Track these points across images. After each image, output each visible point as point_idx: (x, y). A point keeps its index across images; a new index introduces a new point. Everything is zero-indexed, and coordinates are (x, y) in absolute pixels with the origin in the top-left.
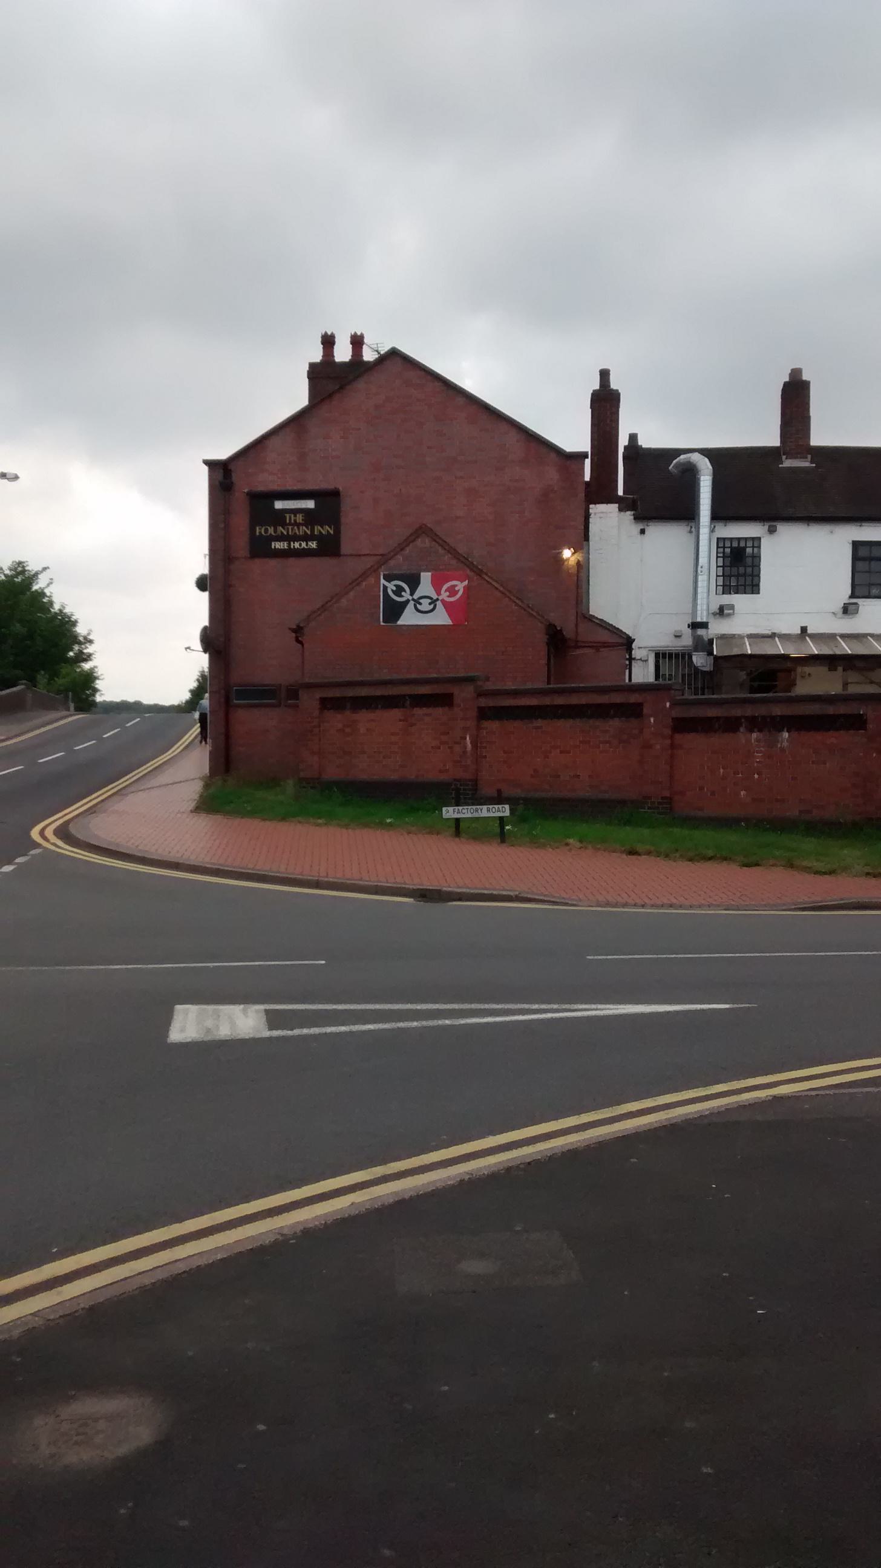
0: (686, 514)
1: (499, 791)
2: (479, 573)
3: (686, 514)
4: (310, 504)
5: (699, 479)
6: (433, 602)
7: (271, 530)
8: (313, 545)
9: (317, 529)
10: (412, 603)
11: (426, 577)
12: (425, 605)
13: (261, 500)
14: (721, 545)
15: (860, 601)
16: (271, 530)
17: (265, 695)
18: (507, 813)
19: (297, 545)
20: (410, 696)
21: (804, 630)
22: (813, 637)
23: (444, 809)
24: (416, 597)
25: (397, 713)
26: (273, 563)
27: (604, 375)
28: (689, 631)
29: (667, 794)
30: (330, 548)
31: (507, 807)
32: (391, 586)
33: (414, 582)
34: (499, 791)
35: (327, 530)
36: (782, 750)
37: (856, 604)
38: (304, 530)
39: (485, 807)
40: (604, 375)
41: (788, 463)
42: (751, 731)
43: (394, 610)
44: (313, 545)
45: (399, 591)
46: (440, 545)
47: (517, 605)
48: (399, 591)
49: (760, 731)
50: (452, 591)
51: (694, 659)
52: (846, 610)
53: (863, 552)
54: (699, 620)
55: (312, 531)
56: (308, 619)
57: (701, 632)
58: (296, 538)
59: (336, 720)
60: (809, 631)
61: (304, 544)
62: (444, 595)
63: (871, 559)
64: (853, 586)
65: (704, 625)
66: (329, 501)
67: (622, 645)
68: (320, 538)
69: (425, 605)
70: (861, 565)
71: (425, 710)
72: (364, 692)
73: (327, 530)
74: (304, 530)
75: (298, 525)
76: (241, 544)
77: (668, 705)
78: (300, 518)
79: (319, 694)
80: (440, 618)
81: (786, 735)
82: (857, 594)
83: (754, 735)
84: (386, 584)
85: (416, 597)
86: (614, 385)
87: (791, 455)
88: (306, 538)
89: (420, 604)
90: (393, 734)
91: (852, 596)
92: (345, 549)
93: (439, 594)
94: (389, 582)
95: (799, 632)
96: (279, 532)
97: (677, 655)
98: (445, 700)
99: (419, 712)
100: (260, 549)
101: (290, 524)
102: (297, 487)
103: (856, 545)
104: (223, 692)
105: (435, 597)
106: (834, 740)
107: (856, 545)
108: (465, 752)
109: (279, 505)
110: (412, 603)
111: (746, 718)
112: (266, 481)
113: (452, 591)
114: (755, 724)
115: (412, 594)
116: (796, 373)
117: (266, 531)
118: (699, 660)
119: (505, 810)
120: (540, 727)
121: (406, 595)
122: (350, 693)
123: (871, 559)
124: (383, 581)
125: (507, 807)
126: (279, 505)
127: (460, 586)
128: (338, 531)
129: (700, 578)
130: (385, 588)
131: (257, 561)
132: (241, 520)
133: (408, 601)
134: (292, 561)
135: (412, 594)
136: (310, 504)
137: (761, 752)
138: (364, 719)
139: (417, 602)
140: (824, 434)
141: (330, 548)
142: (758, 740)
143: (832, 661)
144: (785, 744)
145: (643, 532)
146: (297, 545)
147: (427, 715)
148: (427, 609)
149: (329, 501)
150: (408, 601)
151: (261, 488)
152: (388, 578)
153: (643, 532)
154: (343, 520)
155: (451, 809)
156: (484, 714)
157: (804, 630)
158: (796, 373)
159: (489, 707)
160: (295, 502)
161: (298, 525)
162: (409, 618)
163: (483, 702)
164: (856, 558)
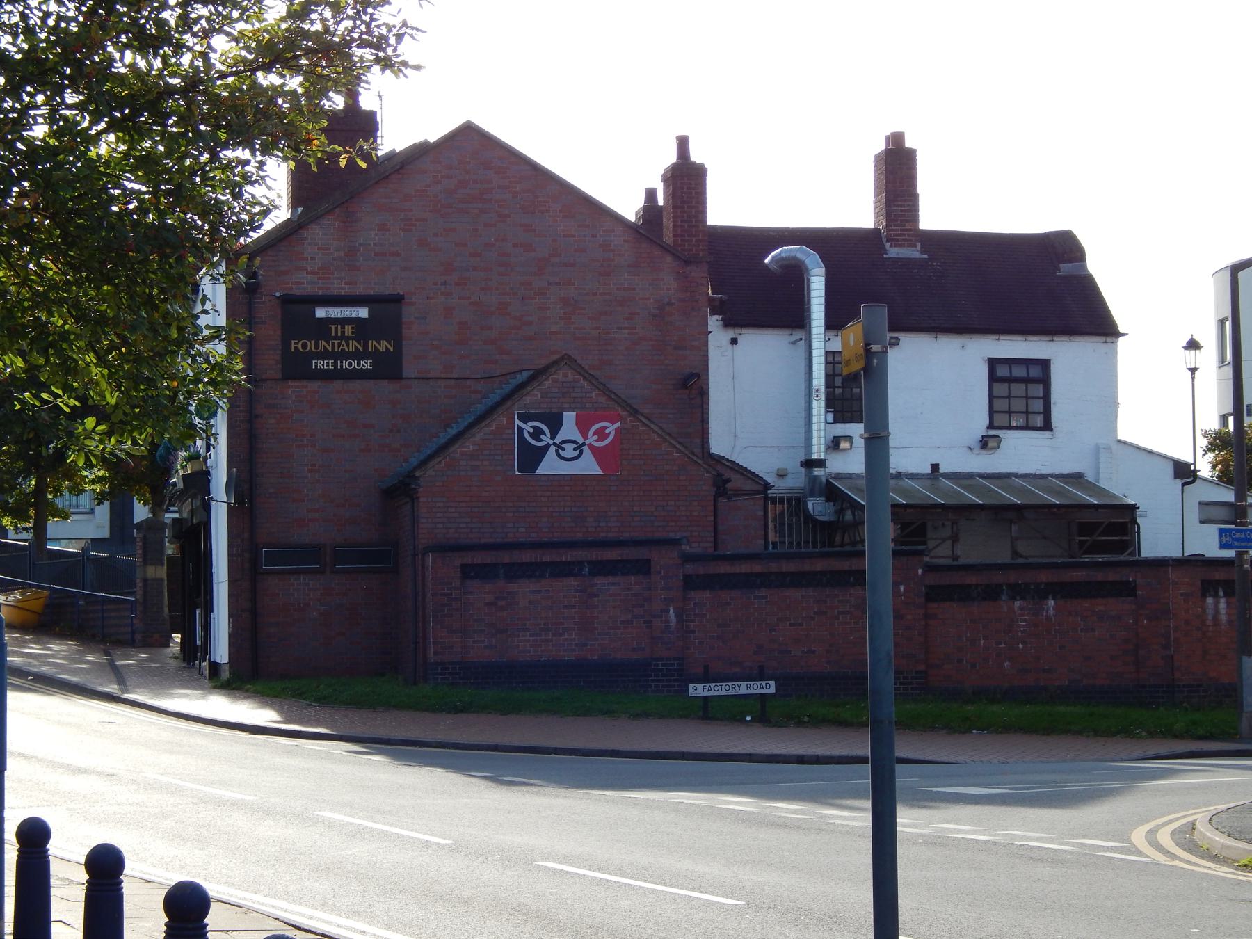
0: (790, 316)
1: (706, 668)
2: (634, 412)
3: (790, 316)
4: (363, 313)
5: (809, 280)
6: (579, 447)
7: (311, 345)
8: (367, 365)
9: (372, 344)
10: (553, 448)
11: (569, 417)
12: (569, 451)
13: (296, 309)
14: (830, 359)
15: (1000, 433)
16: (311, 345)
17: (307, 558)
18: (772, 690)
19: (345, 364)
20: (590, 562)
21: (935, 467)
22: (948, 476)
23: (691, 686)
24: (557, 440)
25: (572, 582)
26: (314, 385)
27: (683, 143)
28: (803, 470)
29: (922, 667)
30: (388, 368)
31: (772, 683)
32: (528, 428)
33: (555, 424)
34: (706, 668)
35: (385, 345)
36: (1048, 618)
37: (997, 437)
38: (353, 345)
39: (744, 684)
40: (683, 143)
41: (893, 252)
42: (1013, 598)
43: (532, 456)
44: (367, 365)
45: (537, 434)
46: (585, 378)
47: (679, 451)
48: (537, 434)
49: (1023, 598)
50: (601, 434)
51: (810, 505)
52: (985, 443)
53: (1002, 371)
54: (815, 456)
55: (366, 346)
56: (423, 463)
57: (817, 472)
58: (344, 356)
59: (481, 593)
60: (942, 470)
61: (354, 364)
62: (592, 439)
63: (1010, 380)
64: (992, 412)
65: (821, 463)
66: (387, 309)
67: (758, 493)
68: (375, 356)
69: (569, 451)
70: (1001, 389)
71: (611, 579)
72: (528, 557)
73: (385, 345)
74: (353, 345)
75: (347, 339)
76: (270, 362)
77: (920, 571)
78: (349, 330)
79: (459, 560)
80: (588, 466)
81: (1052, 603)
82: (996, 424)
83: (1017, 604)
84: (522, 425)
85: (557, 440)
86: (696, 156)
87: (895, 242)
88: (357, 356)
89: (575, 449)
90: (566, 607)
91: (991, 426)
92: (409, 369)
93: (586, 438)
94: (525, 423)
95: (929, 470)
96: (321, 348)
97: (790, 499)
98: (643, 568)
99: (600, 581)
100: (296, 368)
101: (336, 337)
102: (345, 291)
103: (993, 363)
104: (247, 555)
105: (581, 440)
106: (1101, 608)
107: (993, 363)
108: (668, 627)
109: (321, 313)
110: (553, 448)
111: (1009, 585)
112: (303, 283)
113: (601, 434)
114: (1017, 591)
115: (553, 438)
116: (1186, 348)
117: (305, 346)
118: (815, 505)
119: (770, 687)
120: (765, 597)
121: (546, 439)
122: (505, 557)
123: (1010, 380)
124: (517, 422)
125: (772, 683)
126: (321, 313)
127: (611, 428)
128: (398, 347)
129: (815, 404)
130: (520, 430)
131: (292, 383)
132: (270, 332)
133: (548, 446)
134: (338, 384)
135: (553, 438)
136: (363, 313)
137: (1025, 620)
138: (525, 590)
139: (559, 447)
140: (938, 212)
141: (388, 368)
142: (1021, 609)
143: (1002, 514)
144: (1051, 612)
145: (734, 341)
146: (345, 364)
147: (613, 584)
148: (571, 456)
149: (387, 309)
150: (548, 446)
151: (297, 291)
152: (525, 418)
153: (734, 341)
154: (405, 332)
155: (700, 686)
156: (690, 583)
157: (935, 467)
158: (1186, 348)
159: (698, 576)
160: (331, 310)
161: (347, 339)
162: (550, 466)
163: (689, 568)
164: (993, 378)
